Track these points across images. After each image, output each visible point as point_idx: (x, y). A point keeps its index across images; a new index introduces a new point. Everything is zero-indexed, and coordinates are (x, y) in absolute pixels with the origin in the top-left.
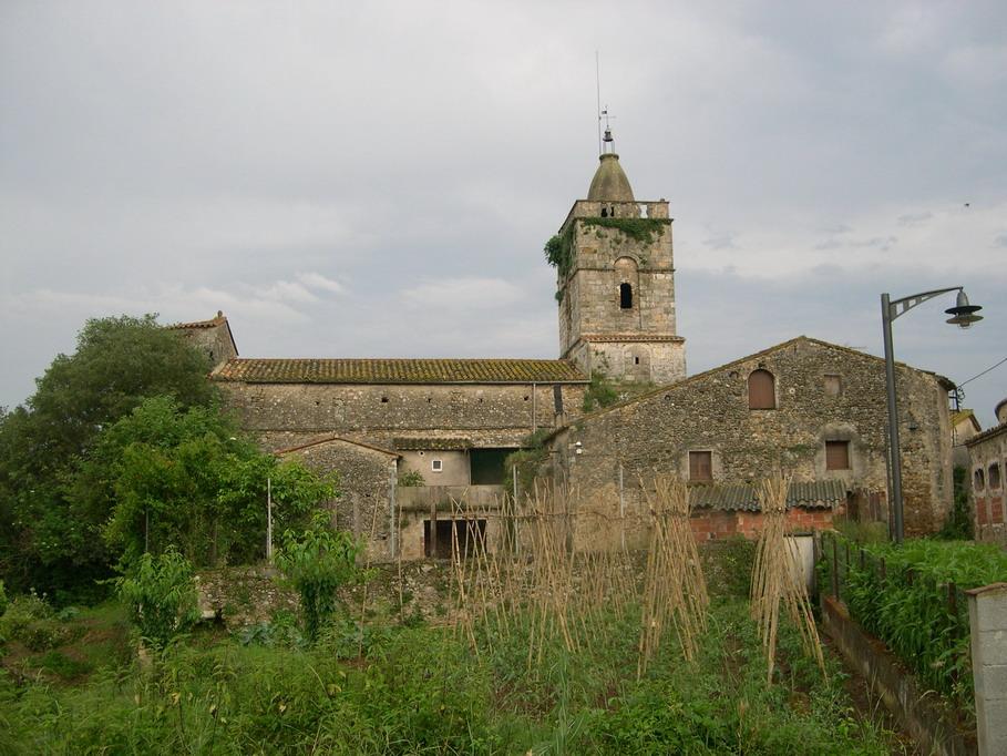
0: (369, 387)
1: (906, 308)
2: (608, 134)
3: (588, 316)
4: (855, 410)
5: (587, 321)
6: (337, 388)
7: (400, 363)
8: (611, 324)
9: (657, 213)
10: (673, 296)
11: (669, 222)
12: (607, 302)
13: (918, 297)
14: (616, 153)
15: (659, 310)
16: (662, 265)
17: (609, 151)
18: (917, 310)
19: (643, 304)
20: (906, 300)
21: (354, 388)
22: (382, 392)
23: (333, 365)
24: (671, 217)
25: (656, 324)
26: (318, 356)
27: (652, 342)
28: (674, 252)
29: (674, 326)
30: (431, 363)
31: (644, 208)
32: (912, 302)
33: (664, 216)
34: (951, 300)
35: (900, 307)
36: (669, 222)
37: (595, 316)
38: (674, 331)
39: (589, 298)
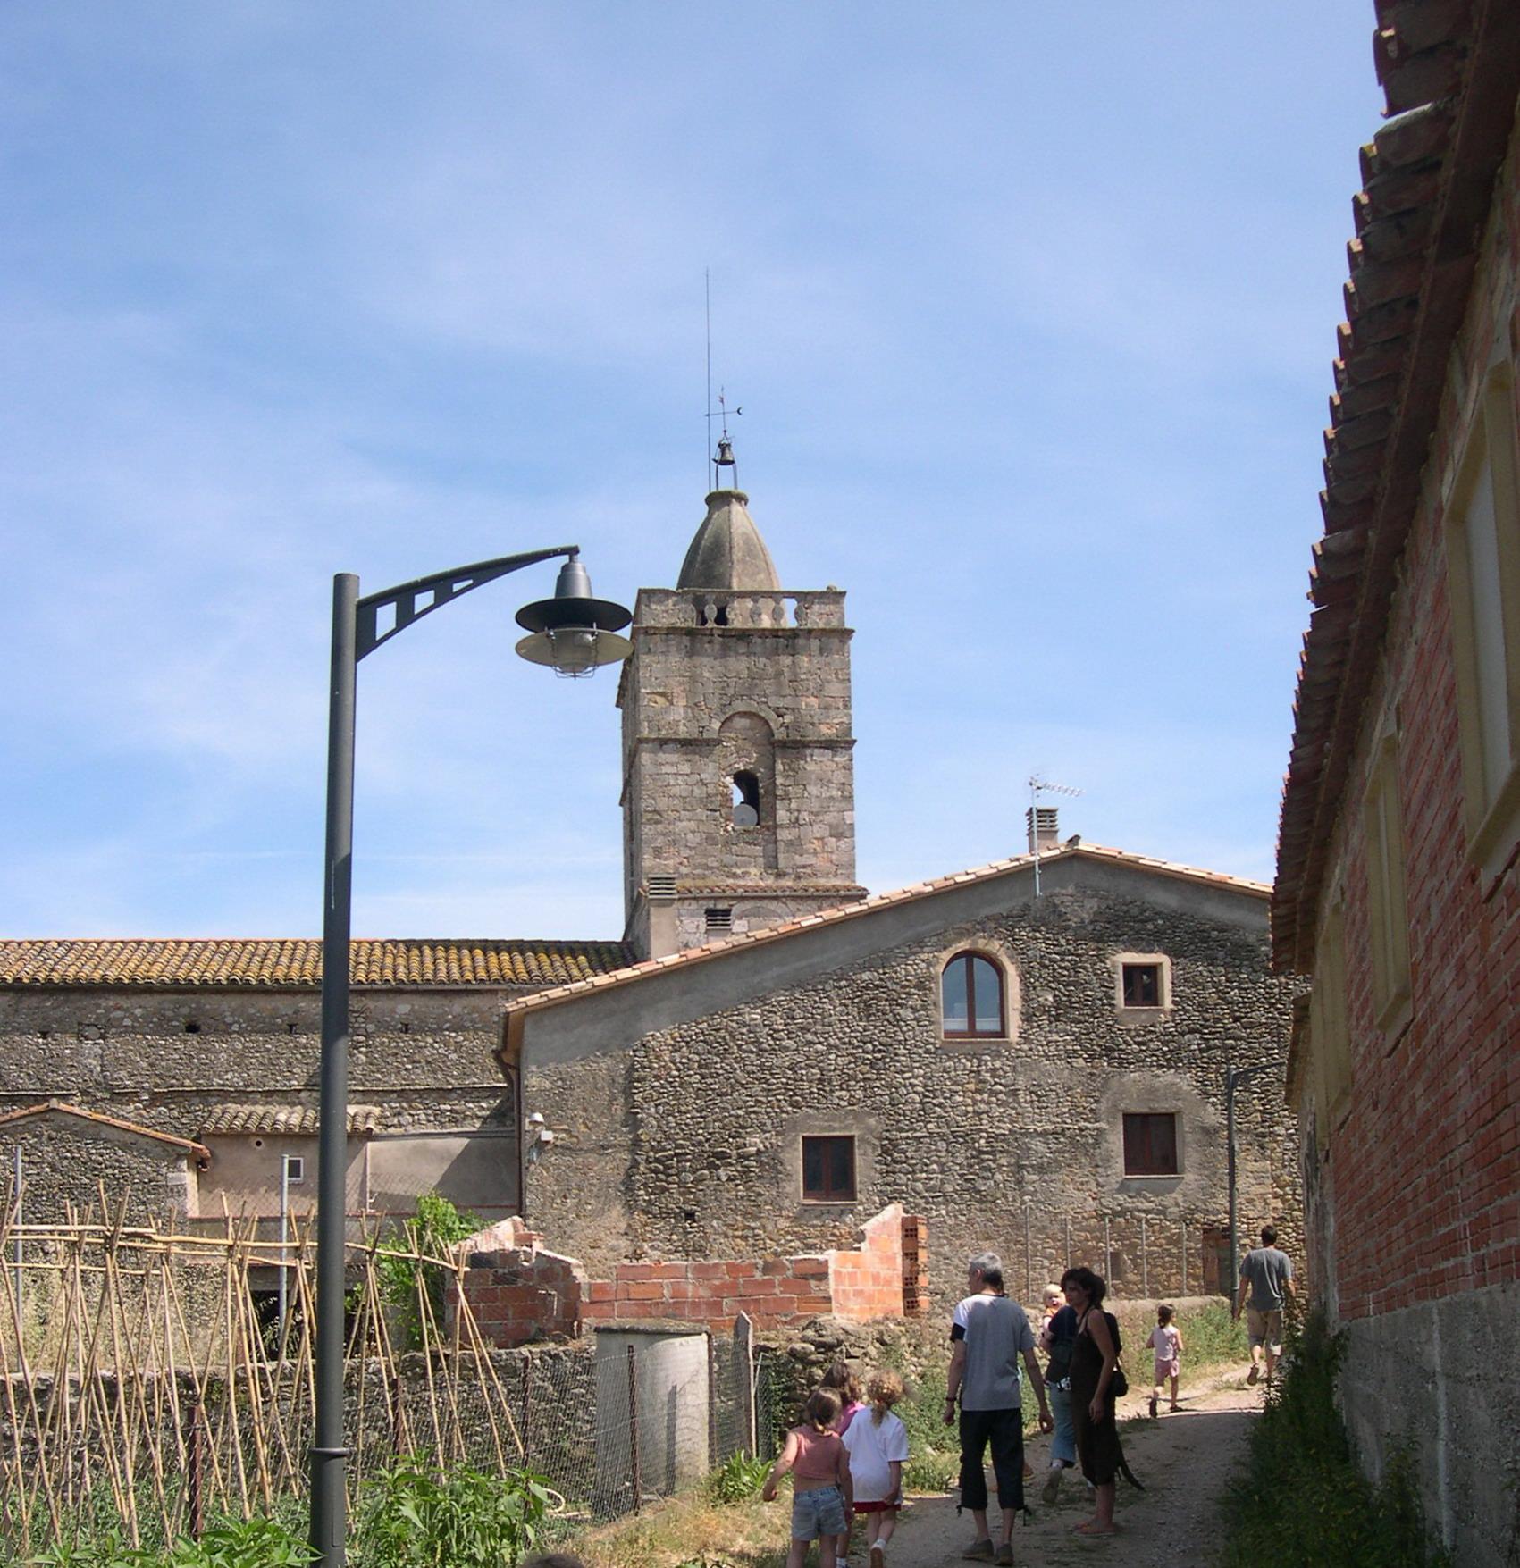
0: (157, 998)
1: (406, 617)
2: (723, 447)
3: (660, 841)
4: (1194, 1041)
5: (657, 852)
6: (87, 1002)
7: (603, 950)
8: (711, 862)
9: (817, 618)
10: (850, 798)
11: (849, 633)
12: (702, 813)
13: (443, 586)
14: (740, 490)
15: (819, 830)
16: (826, 731)
17: (726, 485)
18: (442, 623)
19: (782, 816)
20: (403, 596)
21: (123, 1002)
22: (185, 1011)
23: (299, 953)
24: (848, 626)
25: (813, 860)
26: (490, 938)
27: (794, 898)
28: (854, 702)
29: (852, 865)
30: (610, 951)
31: (790, 605)
32: (424, 600)
33: (835, 623)
34: (538, 585)
35: (386, 616)
36: (849, 633)
37: (674, 842)
38: (851, 876)
39: (662, 804)
